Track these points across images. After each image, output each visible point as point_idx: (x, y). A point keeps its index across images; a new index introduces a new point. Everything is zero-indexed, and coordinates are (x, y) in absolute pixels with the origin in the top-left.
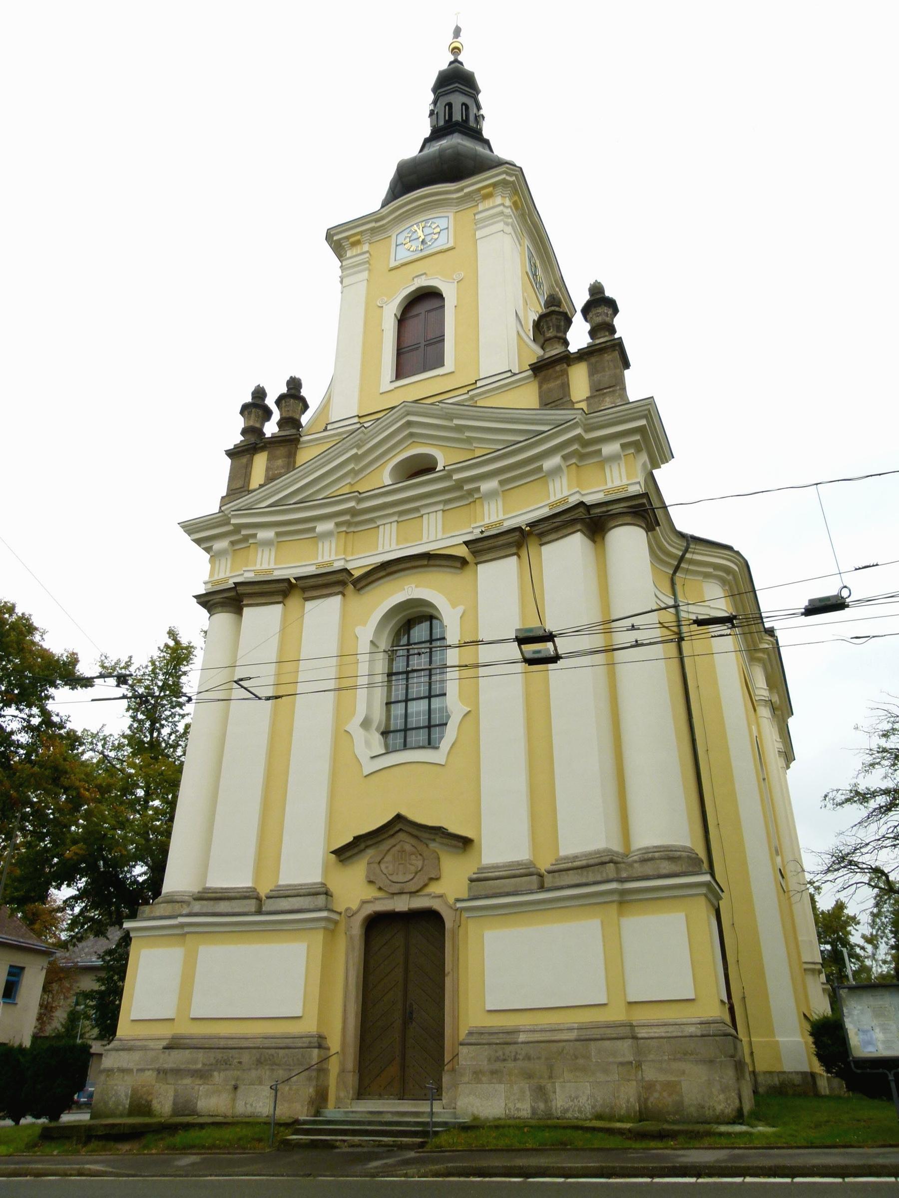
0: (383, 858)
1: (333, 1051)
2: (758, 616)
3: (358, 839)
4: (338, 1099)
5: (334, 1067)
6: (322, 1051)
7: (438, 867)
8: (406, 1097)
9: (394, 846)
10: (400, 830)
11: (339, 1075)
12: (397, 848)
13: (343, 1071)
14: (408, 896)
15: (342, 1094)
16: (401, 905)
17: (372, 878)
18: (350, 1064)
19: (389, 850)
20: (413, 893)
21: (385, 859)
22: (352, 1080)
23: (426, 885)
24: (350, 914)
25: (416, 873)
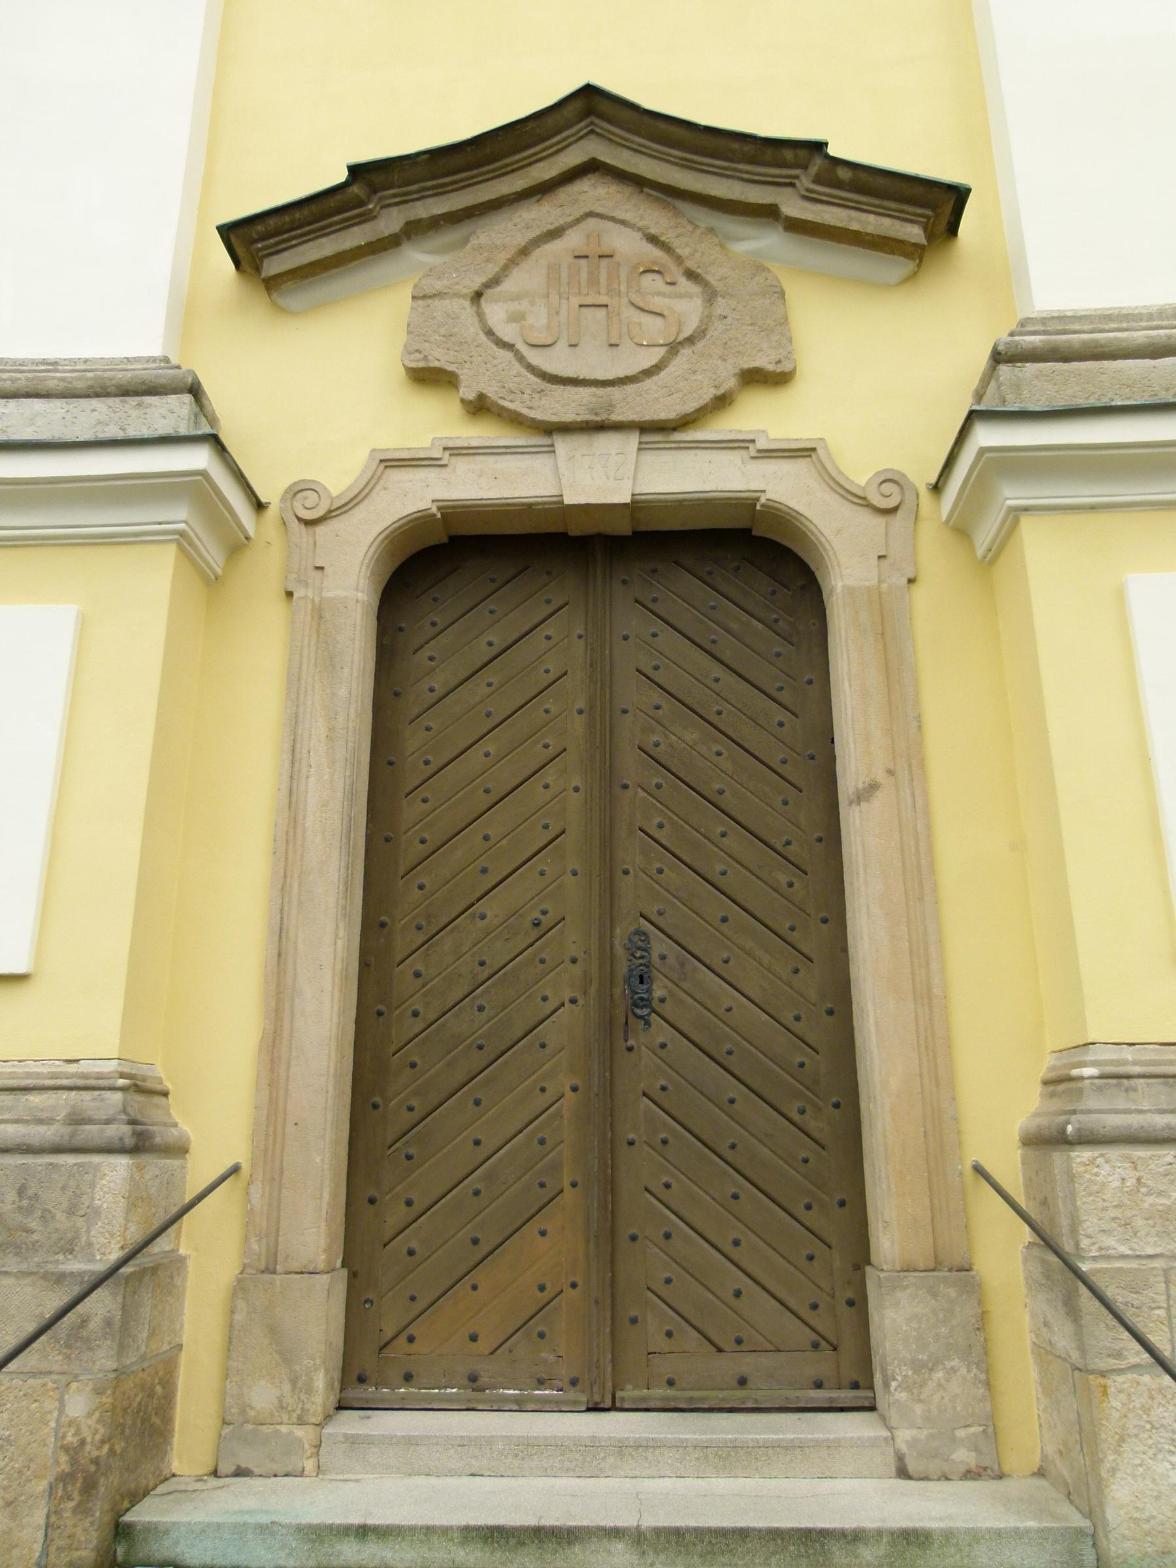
0: (495, 282)
1: (200, 1169)
2: (778, 289)
3: (372, 178)
4: (234, 1422)
5: (210, 1250)
6: (155, 1164)
7: (780, 328)
8: (628, 1393)
9: (555, 234)
10: (591, 167)
11: (240, 1288)
12: (573, 240)
13: (265, 1265)
14: (632, 440)
15: (263, 1396)
16: (598, 477)
17: (439, 358)
18: (313, 1226)
19: (524, 252)
20: (654, 430)
21: (509, 285)
22: (316, 1315)
23: (722, 402)
24: (316, 518)
25: (674, 348)
